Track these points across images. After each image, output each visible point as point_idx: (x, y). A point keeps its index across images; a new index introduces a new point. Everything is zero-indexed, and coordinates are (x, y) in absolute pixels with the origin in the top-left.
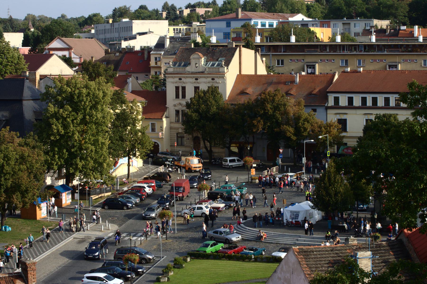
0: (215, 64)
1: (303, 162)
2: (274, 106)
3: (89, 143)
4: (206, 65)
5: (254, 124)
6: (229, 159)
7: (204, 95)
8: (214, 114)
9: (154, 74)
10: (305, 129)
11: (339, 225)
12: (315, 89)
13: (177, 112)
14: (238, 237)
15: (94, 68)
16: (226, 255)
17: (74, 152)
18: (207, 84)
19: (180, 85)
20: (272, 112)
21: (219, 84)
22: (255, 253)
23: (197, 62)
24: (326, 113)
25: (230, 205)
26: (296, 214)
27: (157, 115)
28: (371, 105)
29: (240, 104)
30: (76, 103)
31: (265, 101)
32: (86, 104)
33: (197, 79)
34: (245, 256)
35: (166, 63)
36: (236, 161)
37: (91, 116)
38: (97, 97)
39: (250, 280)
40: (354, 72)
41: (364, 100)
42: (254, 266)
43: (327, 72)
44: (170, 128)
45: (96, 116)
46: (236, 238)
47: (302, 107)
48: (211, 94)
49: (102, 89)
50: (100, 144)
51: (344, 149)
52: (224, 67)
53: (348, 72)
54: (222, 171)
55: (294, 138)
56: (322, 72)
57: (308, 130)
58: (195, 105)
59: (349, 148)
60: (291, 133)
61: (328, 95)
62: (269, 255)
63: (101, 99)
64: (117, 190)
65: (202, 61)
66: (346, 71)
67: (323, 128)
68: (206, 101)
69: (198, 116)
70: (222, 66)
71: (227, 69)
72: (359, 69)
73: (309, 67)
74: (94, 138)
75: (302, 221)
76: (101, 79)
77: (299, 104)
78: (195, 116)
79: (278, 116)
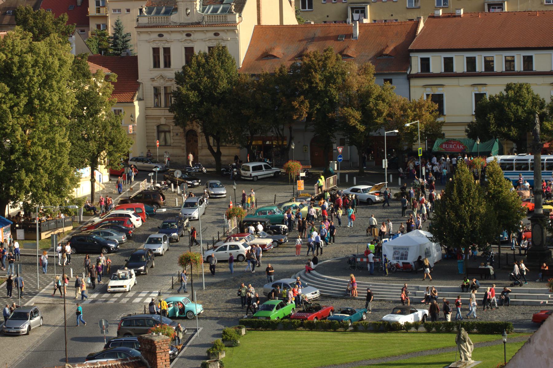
0: (218, 9)
1: (384, 167)
2: (325, 77)
3: (39, 145)
4: (203, 12)
5: (294, 107)
6: (251, 165)
7: (207, 61)
8: (224, 92)
9: (96, 29)
10: (380, 113)
11: (480, 267)
12: (388, 46)
13: (156, 90)
14: (316, 293)
15: (36, 19)
16: (305, 321)
17: (14, 160)
18: (207, 42)
19: (161, 46)
20: (322, 86)
21: (228, 42)
22: (352, 316)
23: (188, 7)
24: (407, 86)
25: (280, 240)
26: (401, 252)
27: (125, 96)
28: (483, 70)
29: (266, 74)
30: (17, 78)
31: (310, 68)
32: (33, 80)
33: (188, 35)
34: (337, 322)
35: (115, 10)
36: (264, 169)
37: (42, 99)
38: (49, 68)
39: (358, 362)
40: (449, 17)
41: (471, 62)
42: (356, 339)
43: (386, 19)
44: (146, 117)
45: (51, 99)
46: (313, 294)
47: (371, 77)
48: (218, 59)
49: (56, 54)
50: (57, 145)
51: (442, 144)
52: (235, 14)
53: (439, 17)
54: (243, 185)
55: (361, 128)
56: (377, 19)
57: (384, 114)
58: (191, 79)
59: (451, 141)
60: (356, 120)
61: (411, 55)
62: (373, 319)
63: (56, 70)
64: (81, 223)
65: (196, 4)
66: (456, 14)
67: (409, 110)
68: (210, 71)
69: (198, 96)
70: (230, 12)
71: (240, 16)
72: (457, 12)
73: (355, 10)
74: (47, 136)
75: (414, 262)
76: (54, 37)
77: (364, 71)
78: (193, 96)
79: (334, 92)
